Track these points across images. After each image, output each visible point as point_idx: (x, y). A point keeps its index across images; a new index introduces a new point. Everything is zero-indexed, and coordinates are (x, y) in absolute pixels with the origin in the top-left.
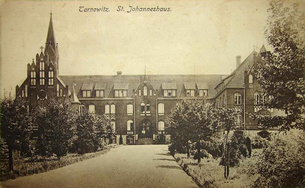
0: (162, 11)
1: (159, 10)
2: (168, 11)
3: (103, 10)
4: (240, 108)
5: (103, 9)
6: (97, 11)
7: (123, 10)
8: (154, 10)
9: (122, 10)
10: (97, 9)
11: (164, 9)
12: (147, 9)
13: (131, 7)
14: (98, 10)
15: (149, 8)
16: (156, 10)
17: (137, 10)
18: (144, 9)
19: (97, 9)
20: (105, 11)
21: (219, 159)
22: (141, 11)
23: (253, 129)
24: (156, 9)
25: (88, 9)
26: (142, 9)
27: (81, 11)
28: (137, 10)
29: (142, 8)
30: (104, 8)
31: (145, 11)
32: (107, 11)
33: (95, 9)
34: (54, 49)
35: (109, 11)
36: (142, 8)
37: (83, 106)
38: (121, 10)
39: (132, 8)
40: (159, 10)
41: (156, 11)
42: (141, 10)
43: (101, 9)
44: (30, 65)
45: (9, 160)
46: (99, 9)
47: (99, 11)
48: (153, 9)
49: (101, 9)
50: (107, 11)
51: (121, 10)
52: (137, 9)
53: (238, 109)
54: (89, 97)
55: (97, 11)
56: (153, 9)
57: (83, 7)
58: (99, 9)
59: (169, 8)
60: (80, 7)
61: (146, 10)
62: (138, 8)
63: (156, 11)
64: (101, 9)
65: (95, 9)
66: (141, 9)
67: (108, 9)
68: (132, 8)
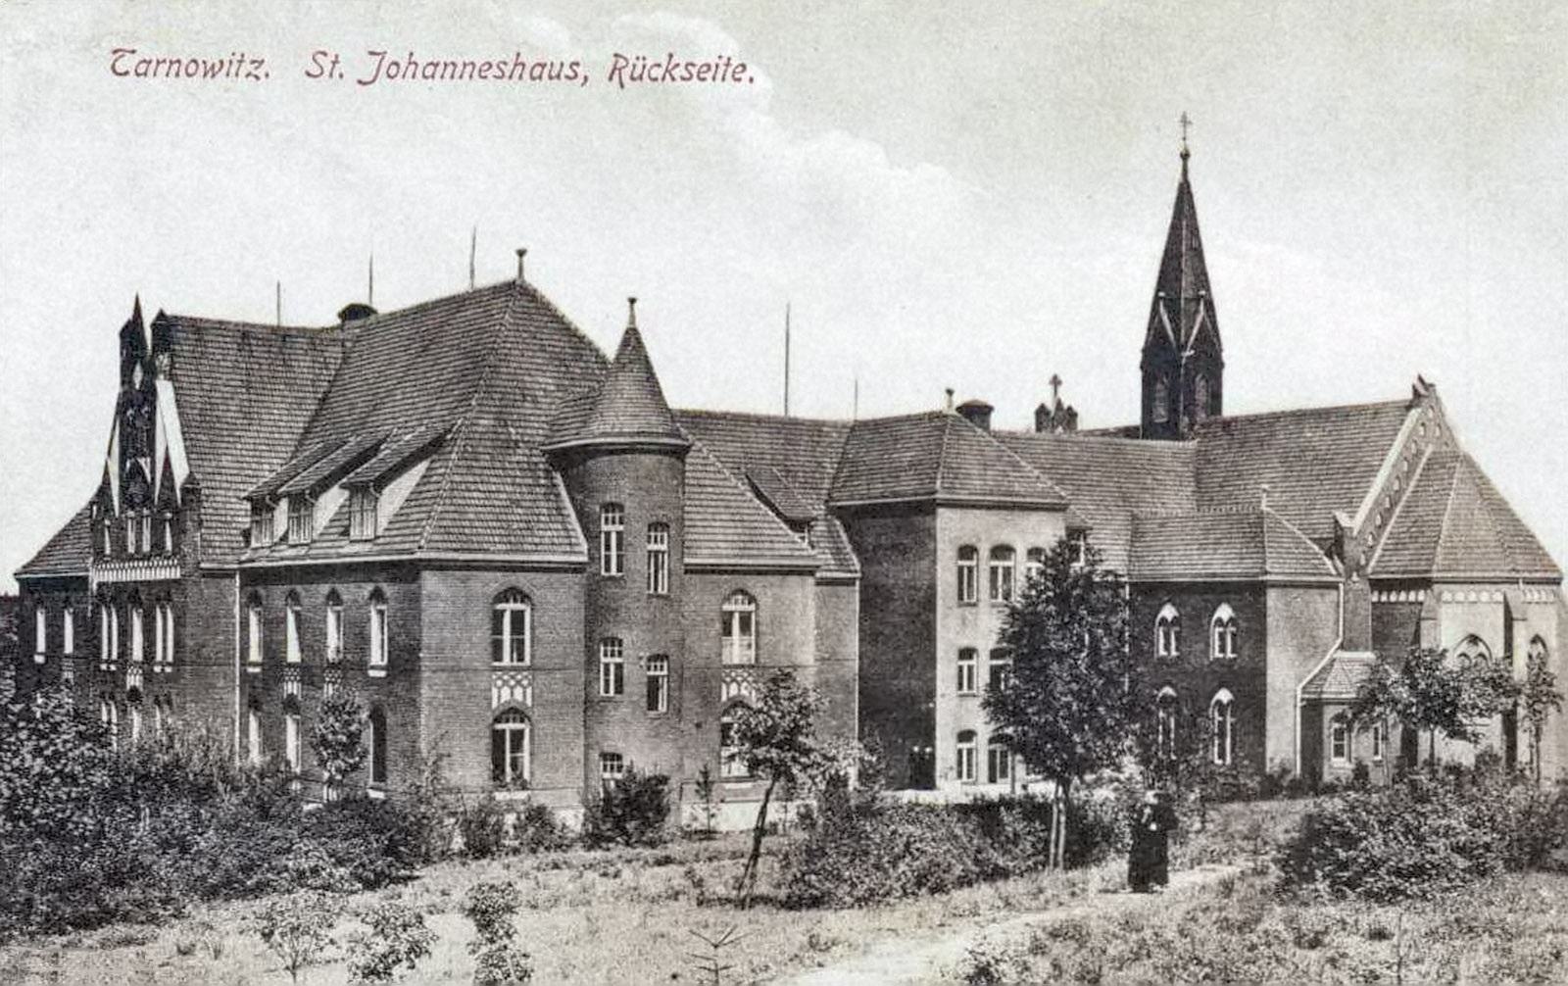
0: (145, 74)
1: (526, 76)
2: (568, 77)
3: (719, 76)
4: (525, 682)
5: (722, 68)
6: (205, 75)
7: (336, 74)
8: (572, 74)
9: (331, 75)
10: (204, 62)
11: (549, 67)
12: (460, 68)
13: (379, 58)
14: (211, 72)
15: (473, 64)
16: (507, 74)
17: (409, 74)
18: (171, 63)
19: (202, 66)
20: (248, 75)
21: (463, 848)
22: (433, 76)
23: (974, 769)
24: (507, 70)
25: (158, 62)
26: (436, 65)
27: (123, 71)
28: (409, 74)
29: (150, 62)
30: (725, 60)
31: (331, 81)
32: (257, 77)
33: (195, 61)
34: (1163, 328)
35: (267, 75)
36: (150, 62)
37: (740, 607)
38: (327, 73)
39: (386, 63)
40: (526, 76)
41: (510, 77)
42: (429, 70)
43: (222, 62)
44: (1048, 413)
45: (1172, 761)
46: (213, 66)
47: (213, 76)
48: (491, 66)
49: (222, 62)
50: (257, 77)
51: (327, 73)
52: (516, 65)
53: (512, 688)
54: (433, 569)
55: (205, 75)
56: (495, 71)
57: (133, 52)
58: (213, 66)
59: (577, 64)
60: (115, 52)
61: (457, 74)
62: (413, 59)
63: (510, 77)
64: (226, 65)
65: (190, 71)
66: (144, 66)
67: (263, 61)
68: (386, 63)
